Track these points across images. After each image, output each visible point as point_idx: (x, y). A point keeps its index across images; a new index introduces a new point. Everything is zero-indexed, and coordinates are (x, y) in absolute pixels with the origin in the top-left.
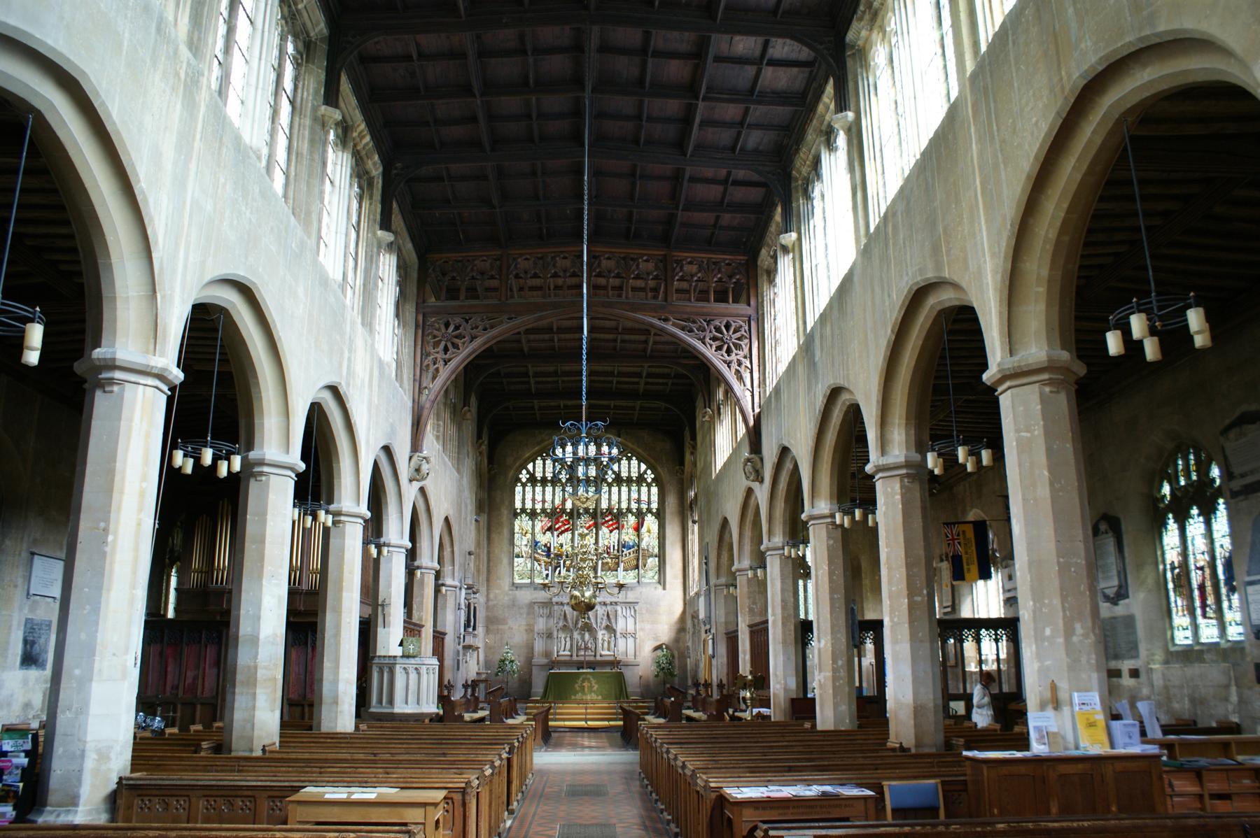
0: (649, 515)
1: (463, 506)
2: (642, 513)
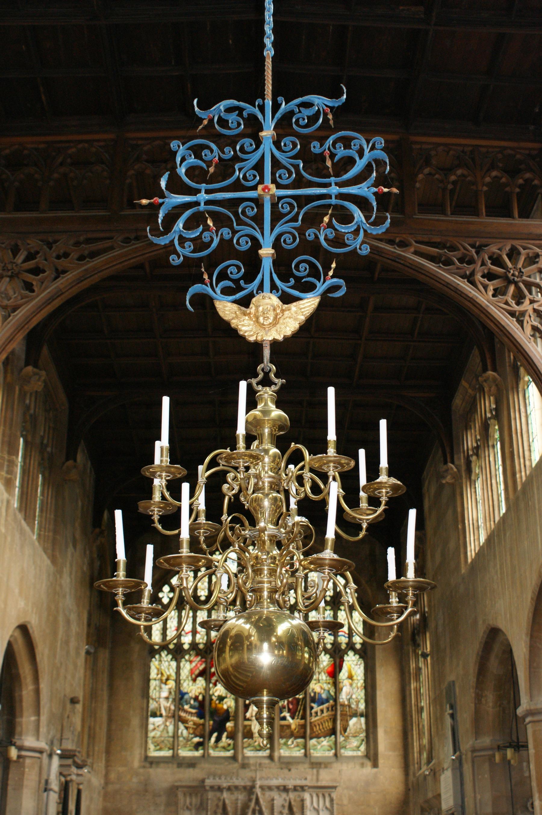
0: (351, 653)
1: (61, 619)
2: (340, 650)
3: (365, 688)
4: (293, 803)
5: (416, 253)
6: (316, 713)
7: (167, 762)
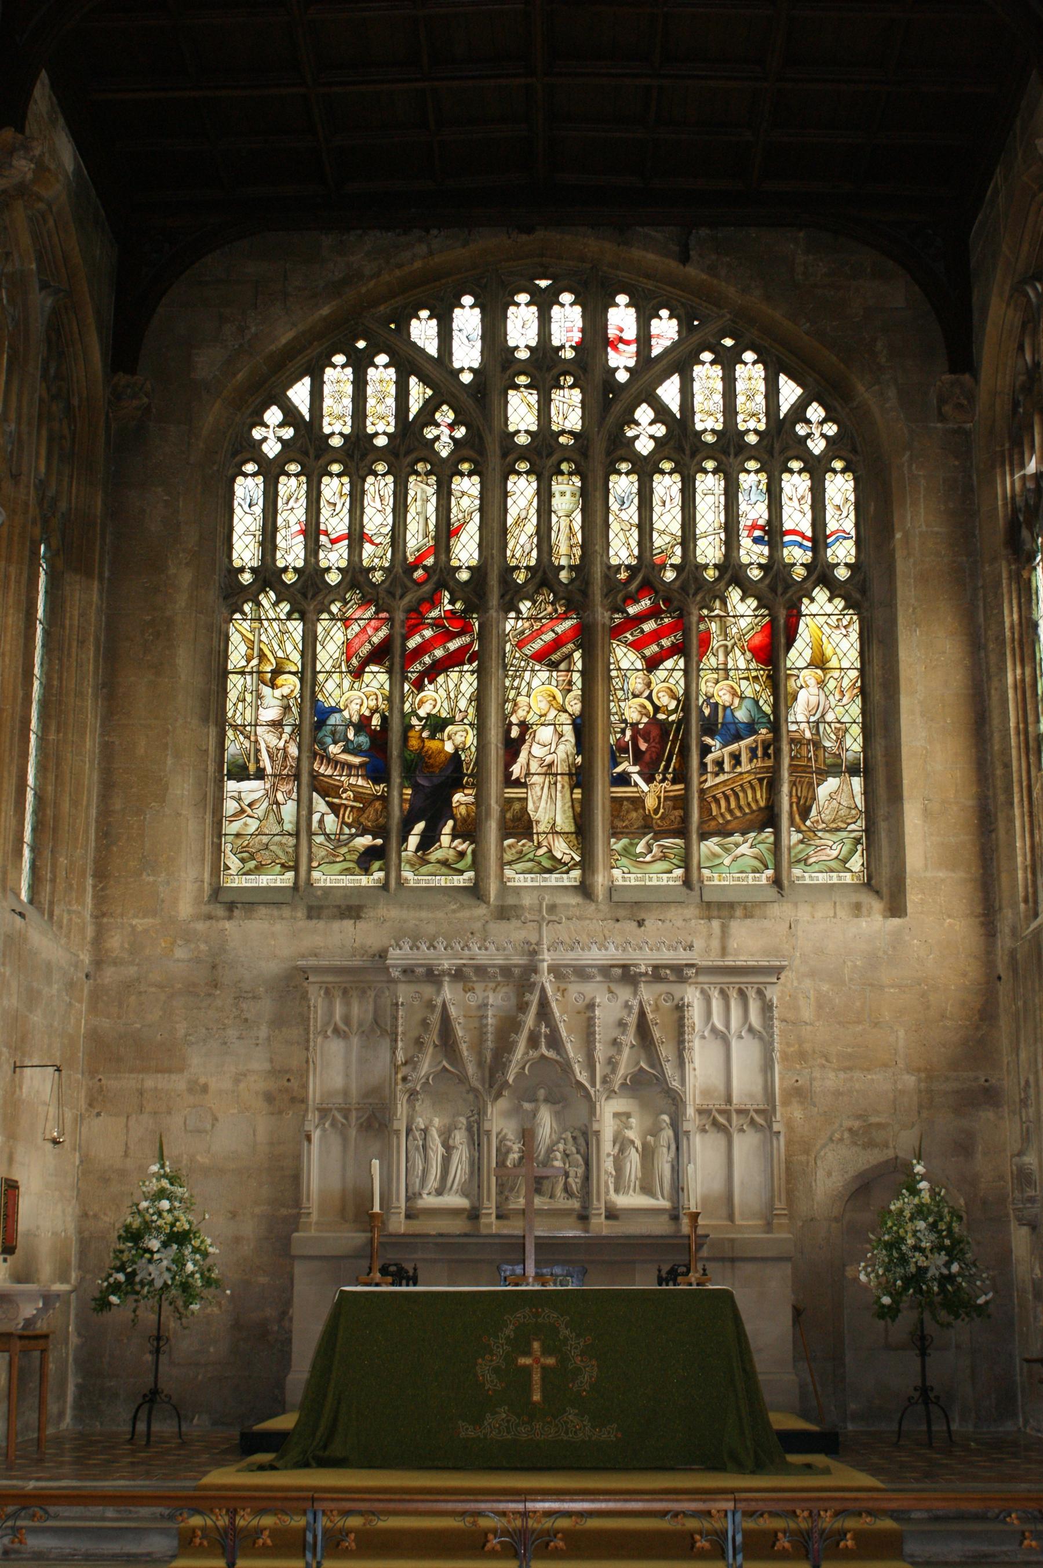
0: (821, 595)
3: (863, 692)
6: (719, 764)
7: (278, 904)
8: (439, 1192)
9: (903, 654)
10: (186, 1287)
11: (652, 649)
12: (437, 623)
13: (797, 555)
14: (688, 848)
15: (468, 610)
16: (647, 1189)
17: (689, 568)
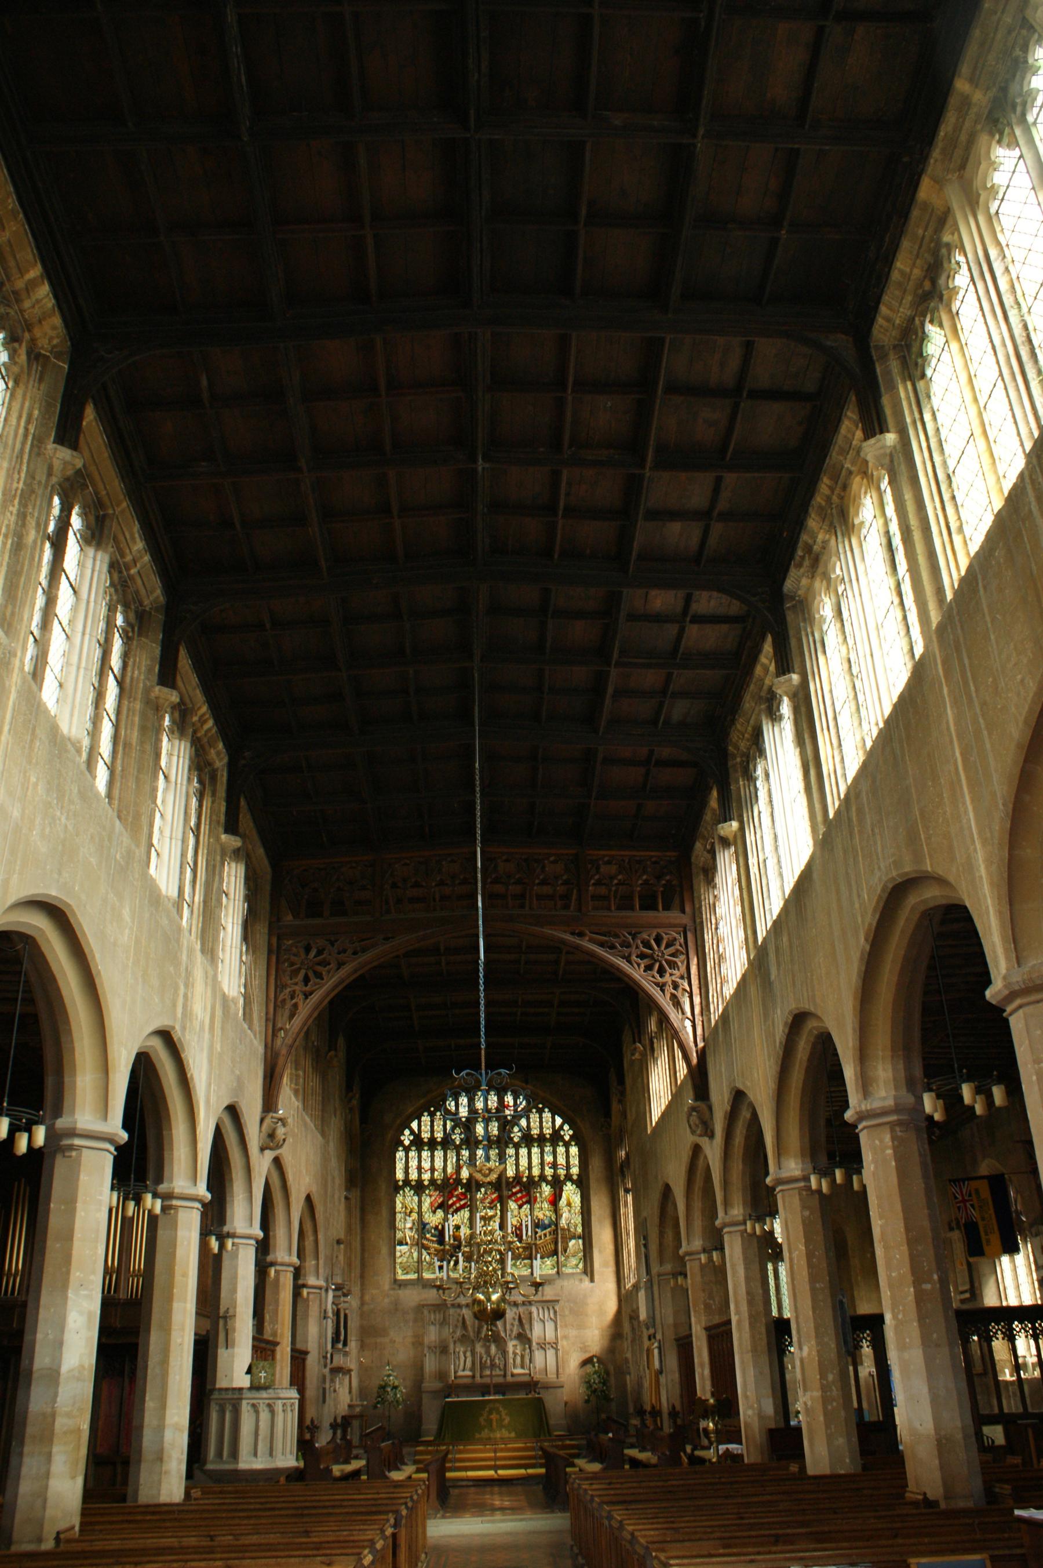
0: (569, 1184)
1: (329, 1178)
3: (582, 1213)
4: (522, 1316)
5: (591, 940)
6: (540, 1237)
7: (413, 1285)
8: (464, 1370)
9: (592, 1203)
10: (397, 1401)
11: (520, 1202)
12: (457, 1196)
13: (562, 1172)
14: (532, 1263)
15: (466, 1191)
16: (522, 1367)
17: (530, 1177)
